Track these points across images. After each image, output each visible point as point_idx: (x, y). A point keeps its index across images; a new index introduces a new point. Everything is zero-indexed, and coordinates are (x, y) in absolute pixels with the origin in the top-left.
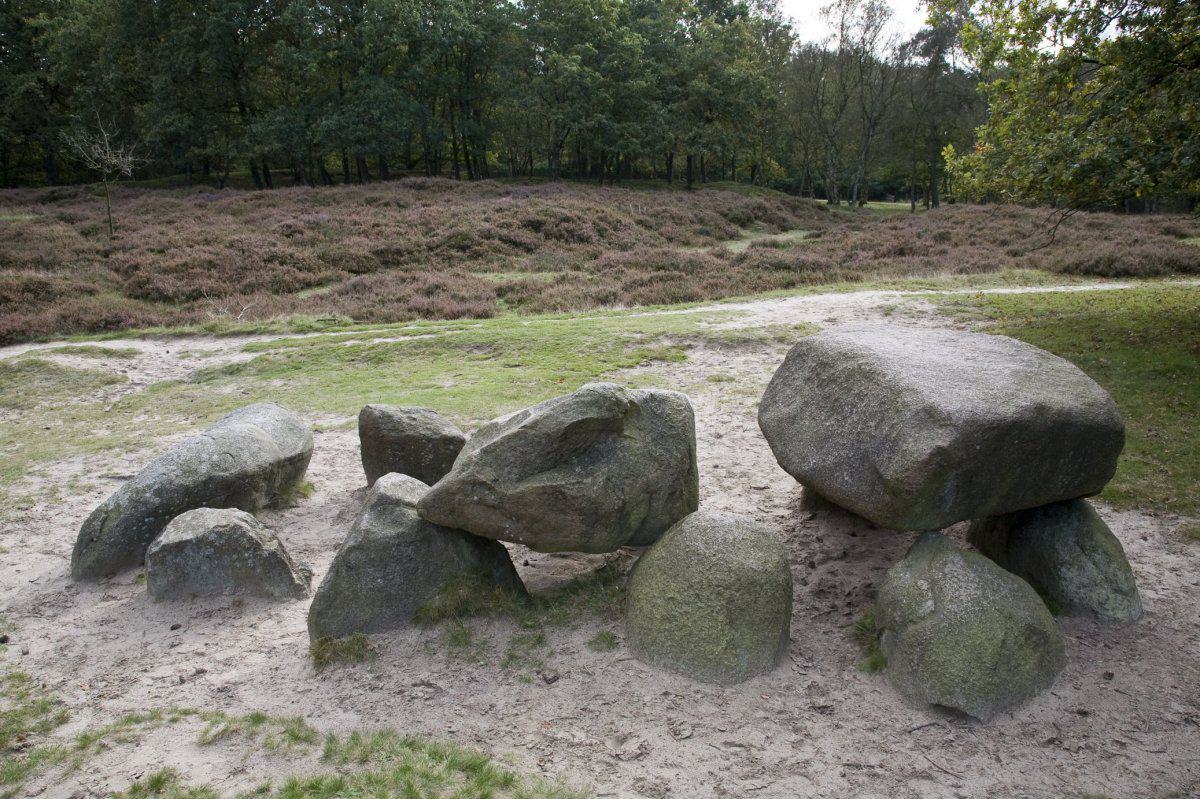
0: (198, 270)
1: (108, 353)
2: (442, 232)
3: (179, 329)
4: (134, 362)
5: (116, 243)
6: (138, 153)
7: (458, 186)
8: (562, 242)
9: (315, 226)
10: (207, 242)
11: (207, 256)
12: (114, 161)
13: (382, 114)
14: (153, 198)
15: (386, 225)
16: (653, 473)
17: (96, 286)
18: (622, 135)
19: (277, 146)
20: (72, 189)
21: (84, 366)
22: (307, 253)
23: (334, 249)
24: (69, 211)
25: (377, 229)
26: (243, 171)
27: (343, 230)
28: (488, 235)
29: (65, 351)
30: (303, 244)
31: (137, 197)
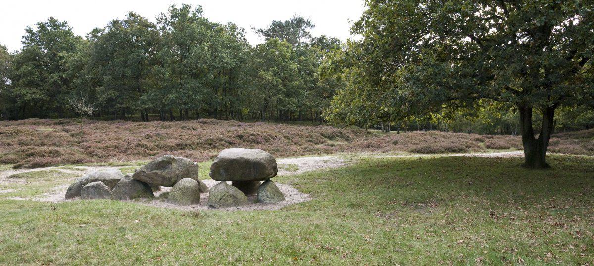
0: (111, 149)
1: (77, 169)
2: (204, 138)
3: (100, 164)
4: (85, 172)
5: (83, 139)
6: (96, 106)
7: (220, 122)
8: (249, 144)
9: (158, 135)
10: (116, 140)
11: (115, 144)
12: (86, 109)
13: (193, 93)
14: (100, 124)
15: (184, 136)
16: (177, 172)
17: (75, 153)
18: (289, 103)
19: (151, 105)
20: (68, 120)
21: (69, 172)
22: (152, 145)
23: (162, 143)
24: (67, 127)
25: (180, 137)
26: (138, 115)
27: (168, 136)
28: (221, 140)
29: (64, 168)
30: (152, 142)
31: (93, 124)
